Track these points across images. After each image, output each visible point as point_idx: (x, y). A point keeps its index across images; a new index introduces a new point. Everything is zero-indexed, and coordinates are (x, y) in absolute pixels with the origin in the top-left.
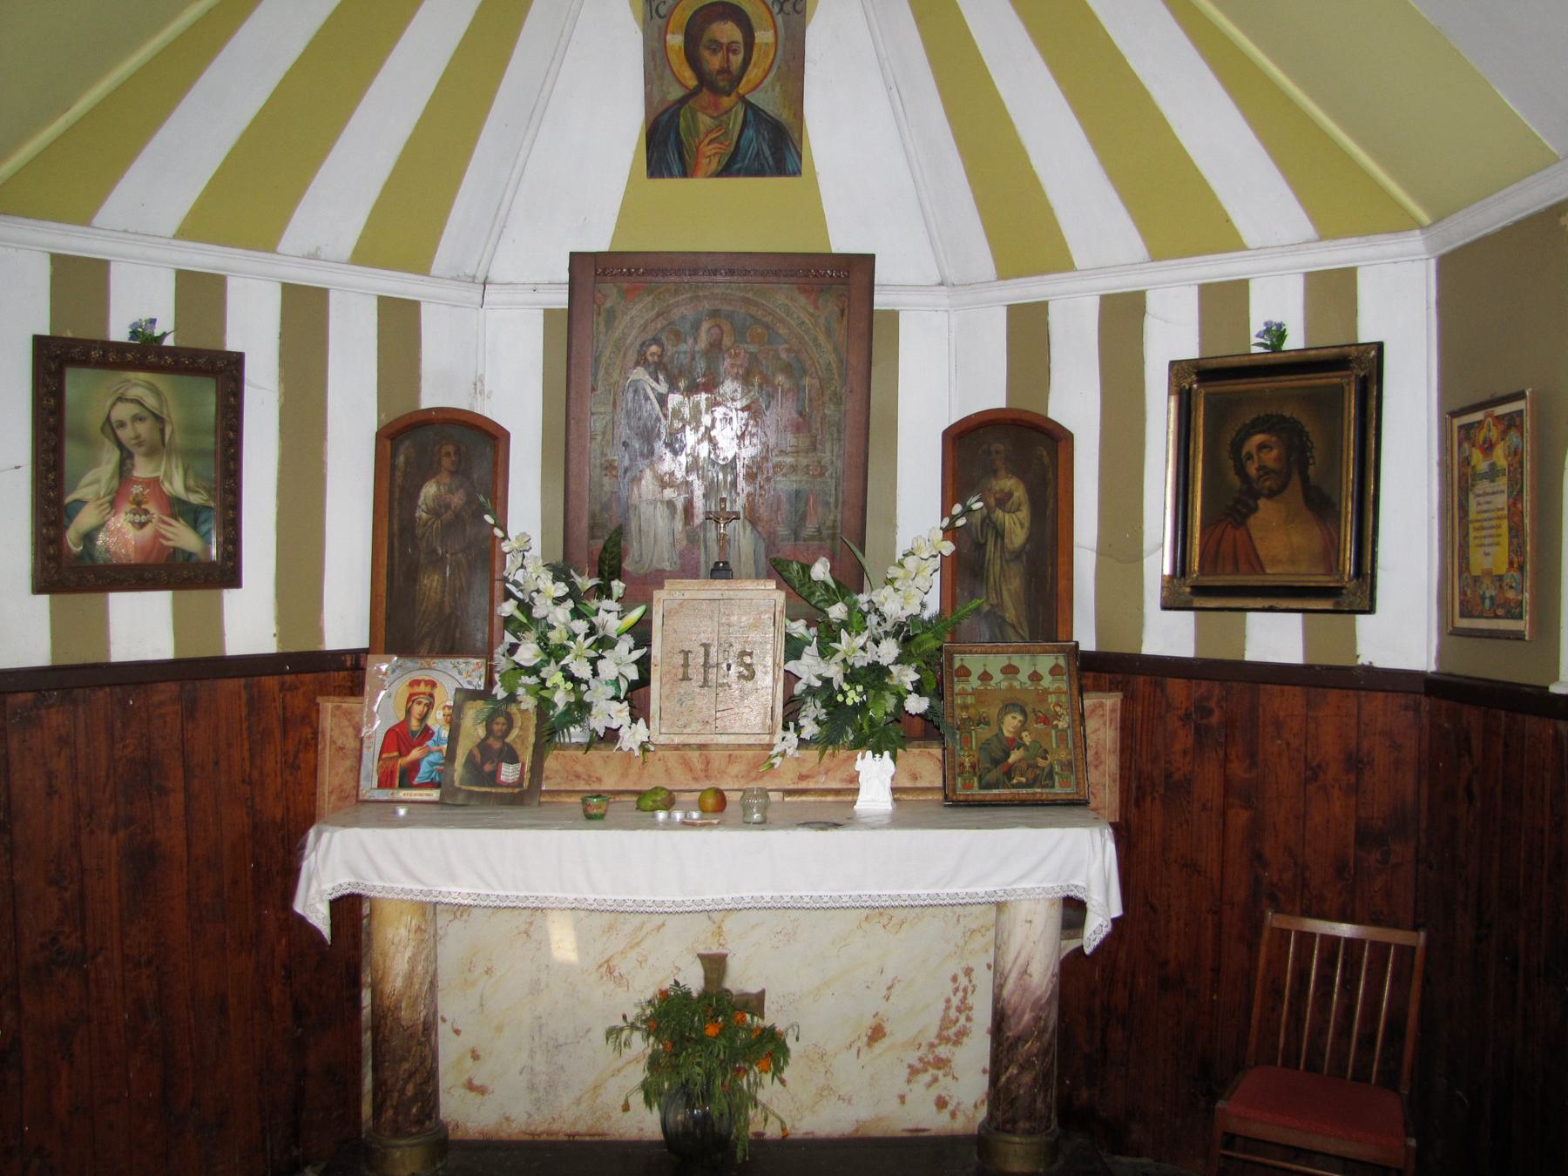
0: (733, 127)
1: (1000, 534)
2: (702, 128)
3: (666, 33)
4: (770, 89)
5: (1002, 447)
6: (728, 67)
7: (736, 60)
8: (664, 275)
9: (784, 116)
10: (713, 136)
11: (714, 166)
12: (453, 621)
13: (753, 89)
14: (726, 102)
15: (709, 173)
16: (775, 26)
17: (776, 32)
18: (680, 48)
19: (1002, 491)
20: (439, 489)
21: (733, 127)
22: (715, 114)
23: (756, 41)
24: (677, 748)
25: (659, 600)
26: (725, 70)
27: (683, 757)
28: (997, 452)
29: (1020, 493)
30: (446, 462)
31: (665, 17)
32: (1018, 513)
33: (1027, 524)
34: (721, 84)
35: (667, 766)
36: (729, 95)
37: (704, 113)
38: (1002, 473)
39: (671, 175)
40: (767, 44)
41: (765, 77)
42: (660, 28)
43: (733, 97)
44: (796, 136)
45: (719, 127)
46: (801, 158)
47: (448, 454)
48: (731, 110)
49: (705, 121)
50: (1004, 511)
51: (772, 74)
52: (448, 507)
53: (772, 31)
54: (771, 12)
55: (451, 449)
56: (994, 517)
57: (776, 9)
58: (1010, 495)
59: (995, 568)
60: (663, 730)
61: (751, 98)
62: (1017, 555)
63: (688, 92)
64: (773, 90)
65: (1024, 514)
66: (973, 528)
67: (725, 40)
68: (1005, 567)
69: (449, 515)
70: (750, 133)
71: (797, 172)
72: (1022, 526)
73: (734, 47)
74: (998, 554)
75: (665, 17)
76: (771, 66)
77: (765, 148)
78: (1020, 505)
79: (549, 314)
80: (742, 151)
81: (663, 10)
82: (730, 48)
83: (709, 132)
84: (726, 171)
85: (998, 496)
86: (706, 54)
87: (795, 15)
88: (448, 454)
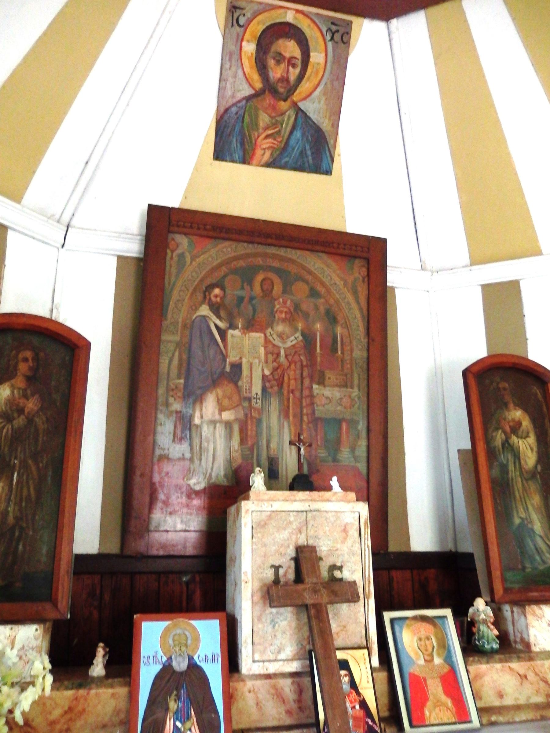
0: (286, 129)
1: (517, 456)
2: (262, 124)
3: (242, 40)
4: (317, 101)
5: (507, 385)
6: (288, 77)
7: (294, 73)
9: (325, 125)
10: (270, 132)
11: (267, 157)
12: (17, 534)
13: (305, 98)
14: (283, 105)
15: (262, 163)
17: (326, 55)
18: (252, 54)
19: (513, 420)
20: (13, 392)
21: (286, 129)
22: (273, 114)
23: (311, 60)
24: (268, 677)
25: (247, 511)
26: (285, 80)
27: (274, 687)
28: (505, 389)
29: (526, 423)
30: (23, 367)
32: (528, 439)
33: (535, 449)
34: (281, 90)
35: (257, 697)
36: (285, 100)
37: (264, 111)
38: (511, 405)
39: (233, 161)
40: (318, 64)
41: (316, 88)
42: (238, 35)
43: (288, 103)
44: (331, 142)
45: (274, 125)
47: (26, 360)
48: (285, 113)
49: (264, 119)
50: (518, 437)
51: (319, 89)
52: (21, 411)
54: (324, 40)
55: (28, 354)
56: (511, 442)
57: (328, 37)
58: (519, 424)
59: (518, 484)
60: (257, 657)
61: (301, 105)
62: (533, 475)
63: (253, 92)
64: (319, 102)
65: (532, 440)
66: (497, 449)
67: (287, 55)
68: (526, 484)
69: (20, 421)
70: (298, 134)
71: (328, 172)
72: (532, 449)
73: (294, 61)
74: (518, 473)
76: (320, 82)
77: (308, 147)
78: (528, 433)
79: (122, 260)
80: (290, 149)
81: (242, 21)
82: (291, 62)
83: (267, 128)
84: (272, 164)
85: (511, 424)
86: (271, 63)
87: (342, 45)
88: (26, 360)
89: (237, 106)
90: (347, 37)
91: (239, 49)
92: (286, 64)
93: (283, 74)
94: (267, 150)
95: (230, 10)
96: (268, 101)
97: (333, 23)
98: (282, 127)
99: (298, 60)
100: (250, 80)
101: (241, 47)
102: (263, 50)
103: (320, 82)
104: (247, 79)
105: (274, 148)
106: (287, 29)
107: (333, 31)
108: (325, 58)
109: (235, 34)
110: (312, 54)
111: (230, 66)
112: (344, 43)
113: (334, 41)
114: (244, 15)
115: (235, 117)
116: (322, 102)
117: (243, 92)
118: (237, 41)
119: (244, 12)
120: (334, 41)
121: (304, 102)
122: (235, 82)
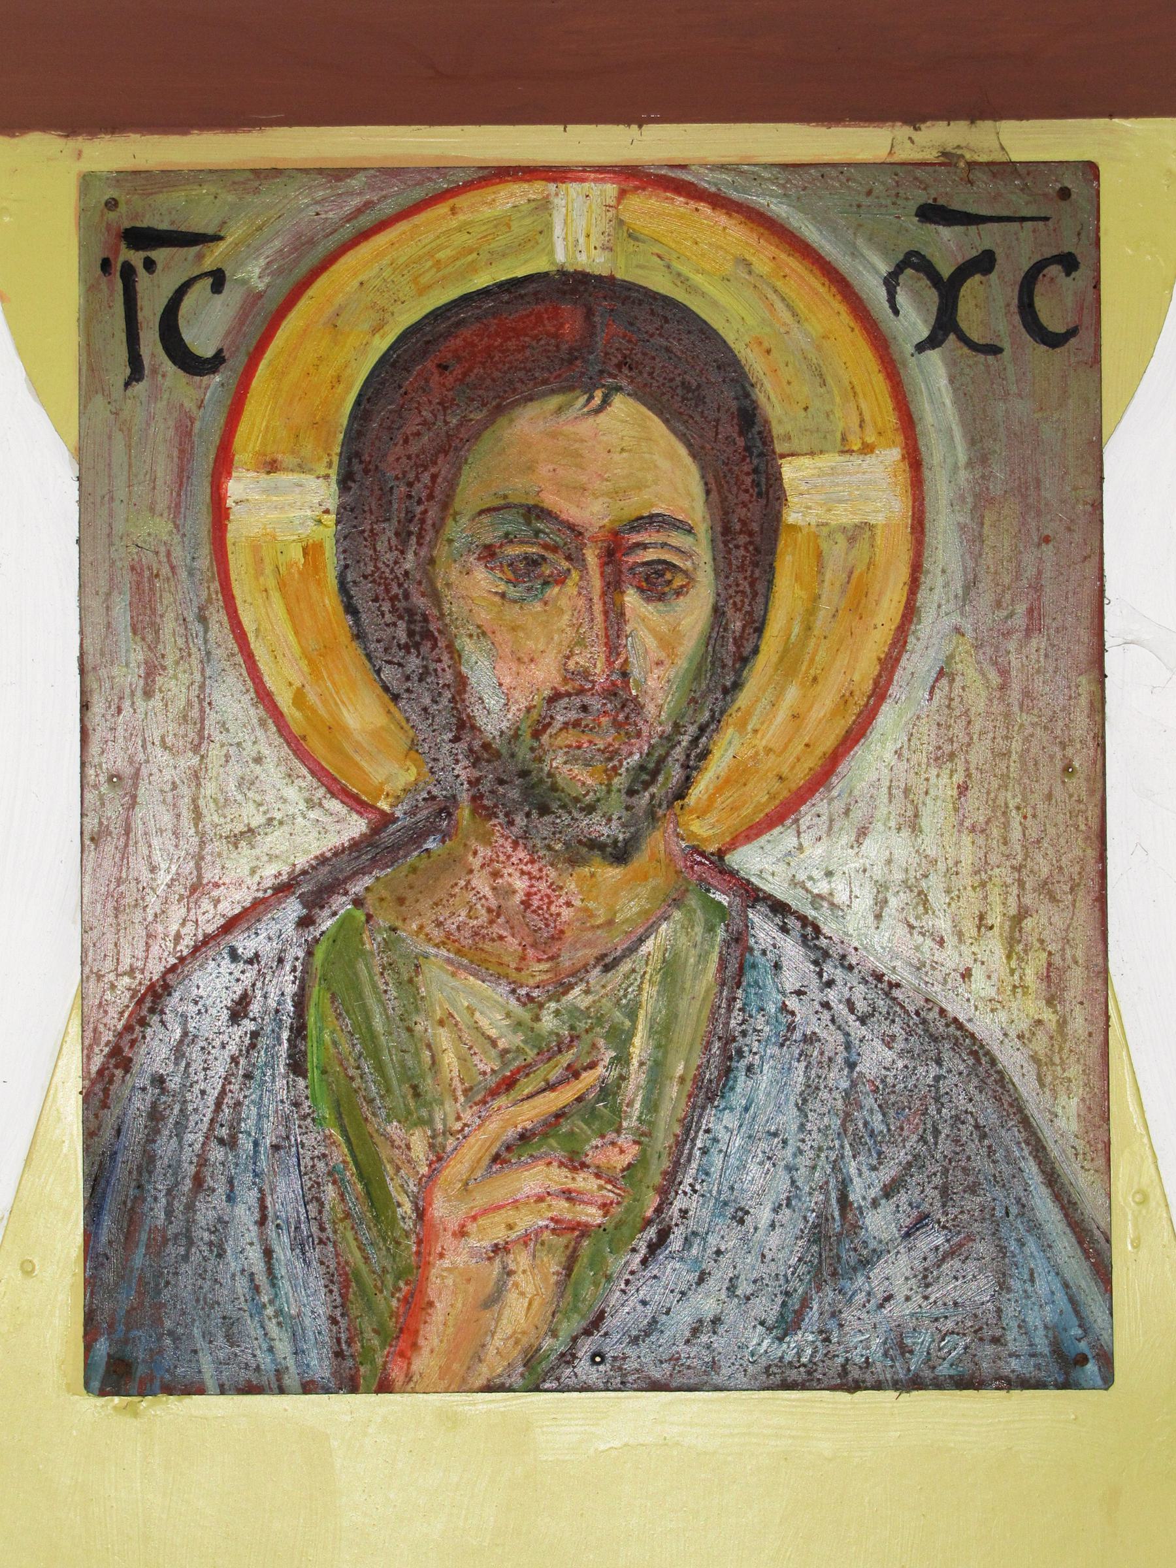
0: (657, 1071)
3: (223, 464)
8: (266, 1207)
16: (908, 423)
17: (914, 462)
18: (311, 551)
23: (792, 516)
31: (215, 363)
40: (858, 533)
42: (185, 432)
46: (1103, 1273)
53: (893, 454)
75: (215, 363)
76: (889, 664)
89: (234, 956)
90: (1070, 286)
91: (202, 524)
92: (597, 583)
93: (580, 660)
94: (521, 1260)
95: (106, 265)
96: (481, 883)
97: (932, 213)
98: (622, 1059)
99: (690, 531)
100: (316, 746)
101: (220, 513)
102: (397, 508)
103: (889, 664)
104: (296, 745)
105: (583, 1230)
106: (571, 325)
107: (946, 270)
108: (904, 477)
109: (163, 431)
110: (790, 471)
111: (152, 671)
112: (1053, 340)
113: (964, 339)
114: (218, 280)
115: (238, 1035)
116: (936, 815)
117: (274, 840)
118: (183, 476)
119: (213, 257)
120: (964, 339)
121: (783, 838)
122: (196, 777)
